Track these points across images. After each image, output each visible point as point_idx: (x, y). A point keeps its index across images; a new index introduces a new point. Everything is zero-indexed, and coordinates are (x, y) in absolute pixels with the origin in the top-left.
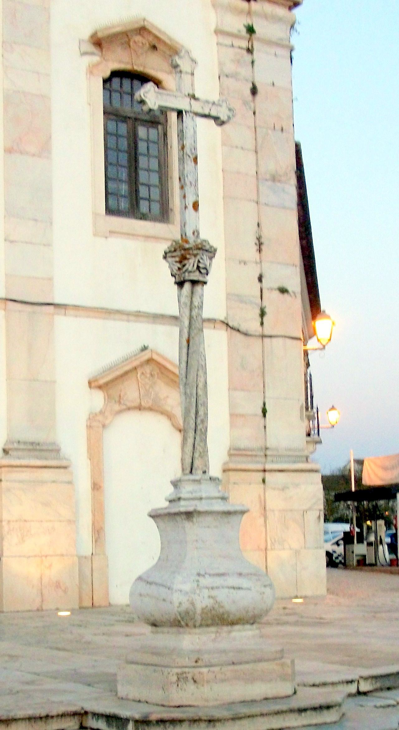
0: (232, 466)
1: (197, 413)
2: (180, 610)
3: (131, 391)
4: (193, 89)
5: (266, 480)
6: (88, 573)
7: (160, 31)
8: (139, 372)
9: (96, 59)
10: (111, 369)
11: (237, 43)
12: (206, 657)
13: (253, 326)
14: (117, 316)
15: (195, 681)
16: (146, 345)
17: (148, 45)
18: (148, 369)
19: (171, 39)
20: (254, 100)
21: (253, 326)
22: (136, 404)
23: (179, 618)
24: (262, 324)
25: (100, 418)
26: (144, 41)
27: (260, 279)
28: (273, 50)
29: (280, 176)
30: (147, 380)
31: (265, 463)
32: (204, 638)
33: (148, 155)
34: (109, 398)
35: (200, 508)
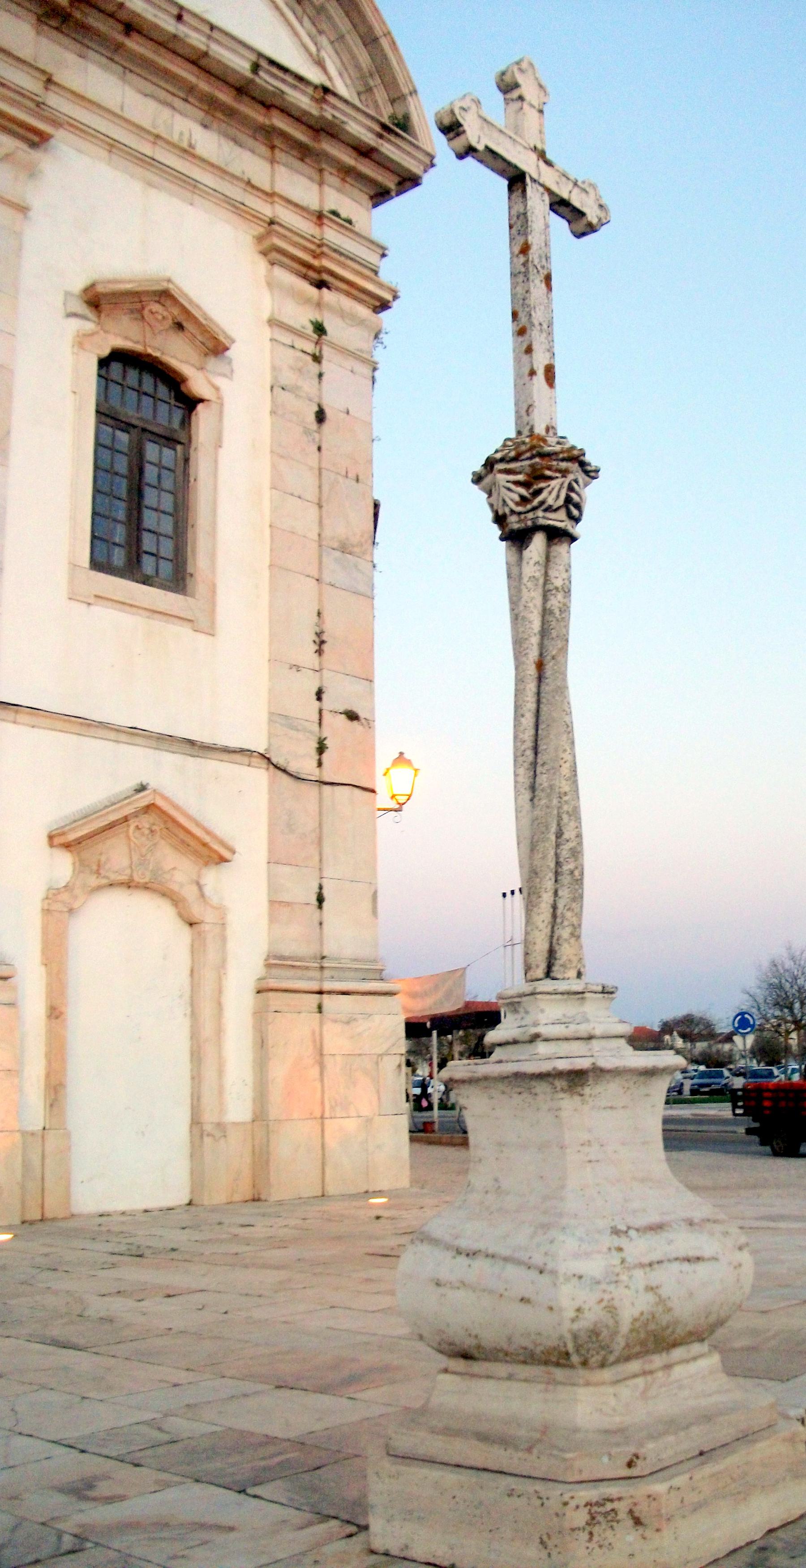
0: (273, 983)
1: (559, 834)
2: (575, 1326)
3: (117, 855)
4: (542, 141)
5: (324, 1008)
6: (36, 1161)
7: (191, 301)
8: (133, 824)
9: (89, 326)
10: (86, 816)
11: (300, 344)
12: (654, 1451)
13: (306, 765)
14: (102, 733)
15: (638, 1522)
16: (144, 783)
17: (170, 322)
18: (146, 821)
19: (205, 315)
20: (319, 431)
21: (306, 765)
22: (124, 878)
23: (570, 1347)
24: (320, 764)
25: (65, 896)
26: (165, 314)
27: (319, 695)
28: (350, 363)
29: (353, 546)
30: (144, 839)
31: (321, 980)
32: (625, 1391)
33: (158, 487)
34: (81, 866)
35: (606, 1062)
